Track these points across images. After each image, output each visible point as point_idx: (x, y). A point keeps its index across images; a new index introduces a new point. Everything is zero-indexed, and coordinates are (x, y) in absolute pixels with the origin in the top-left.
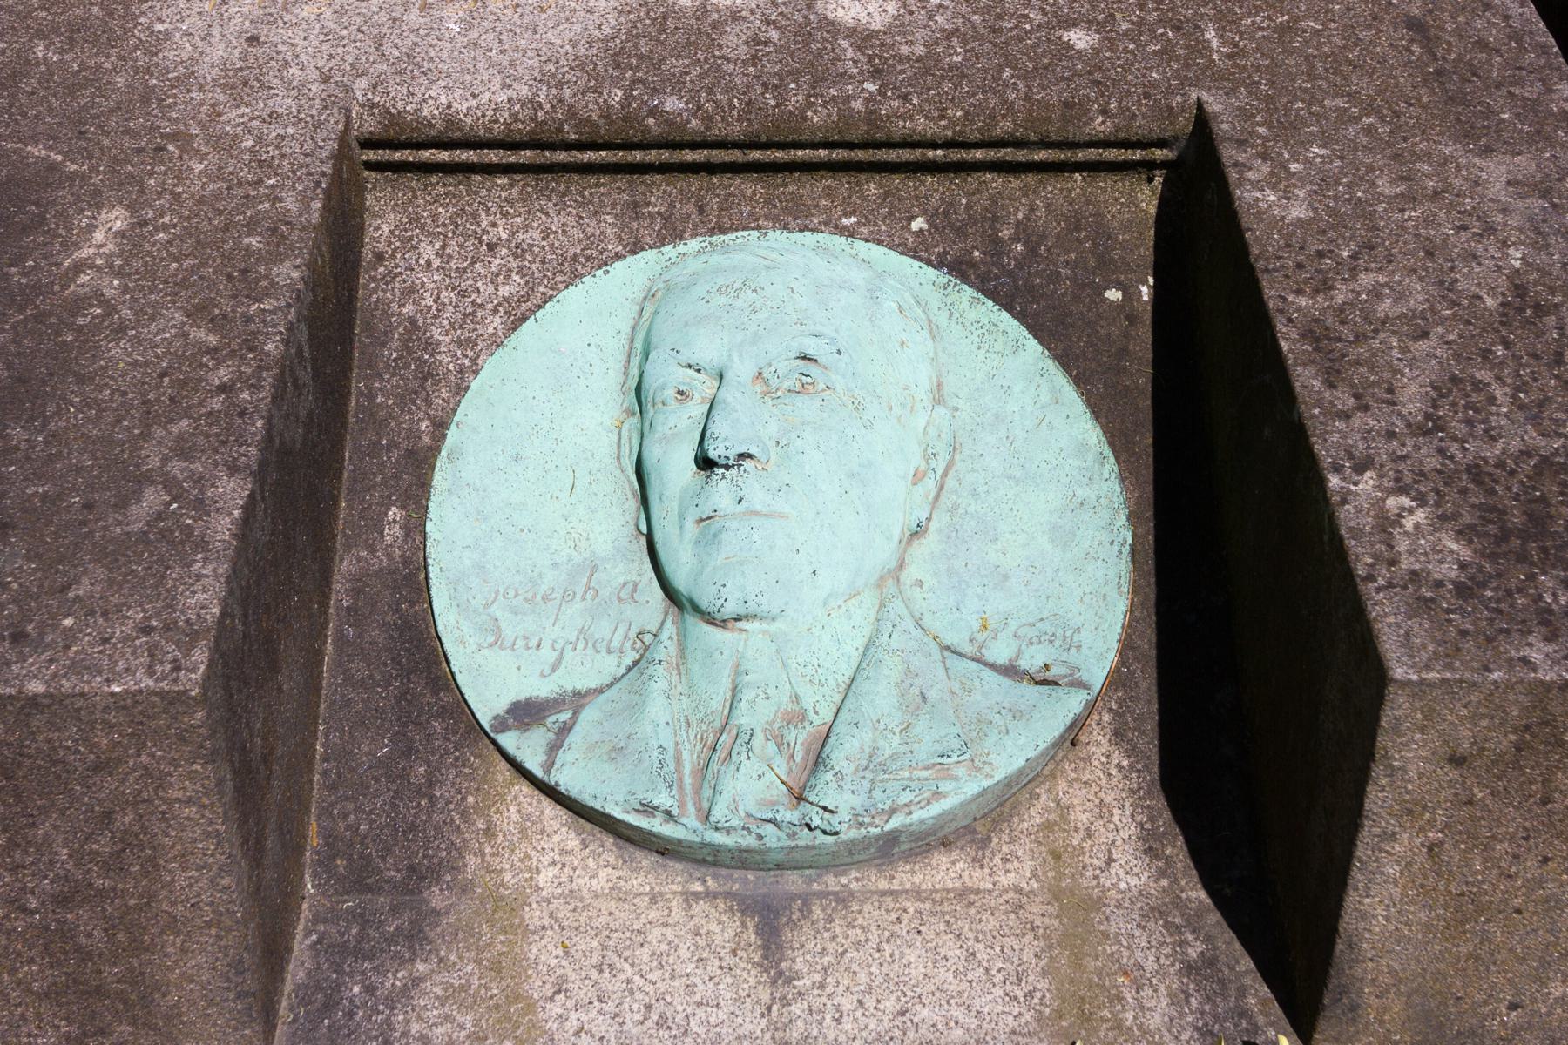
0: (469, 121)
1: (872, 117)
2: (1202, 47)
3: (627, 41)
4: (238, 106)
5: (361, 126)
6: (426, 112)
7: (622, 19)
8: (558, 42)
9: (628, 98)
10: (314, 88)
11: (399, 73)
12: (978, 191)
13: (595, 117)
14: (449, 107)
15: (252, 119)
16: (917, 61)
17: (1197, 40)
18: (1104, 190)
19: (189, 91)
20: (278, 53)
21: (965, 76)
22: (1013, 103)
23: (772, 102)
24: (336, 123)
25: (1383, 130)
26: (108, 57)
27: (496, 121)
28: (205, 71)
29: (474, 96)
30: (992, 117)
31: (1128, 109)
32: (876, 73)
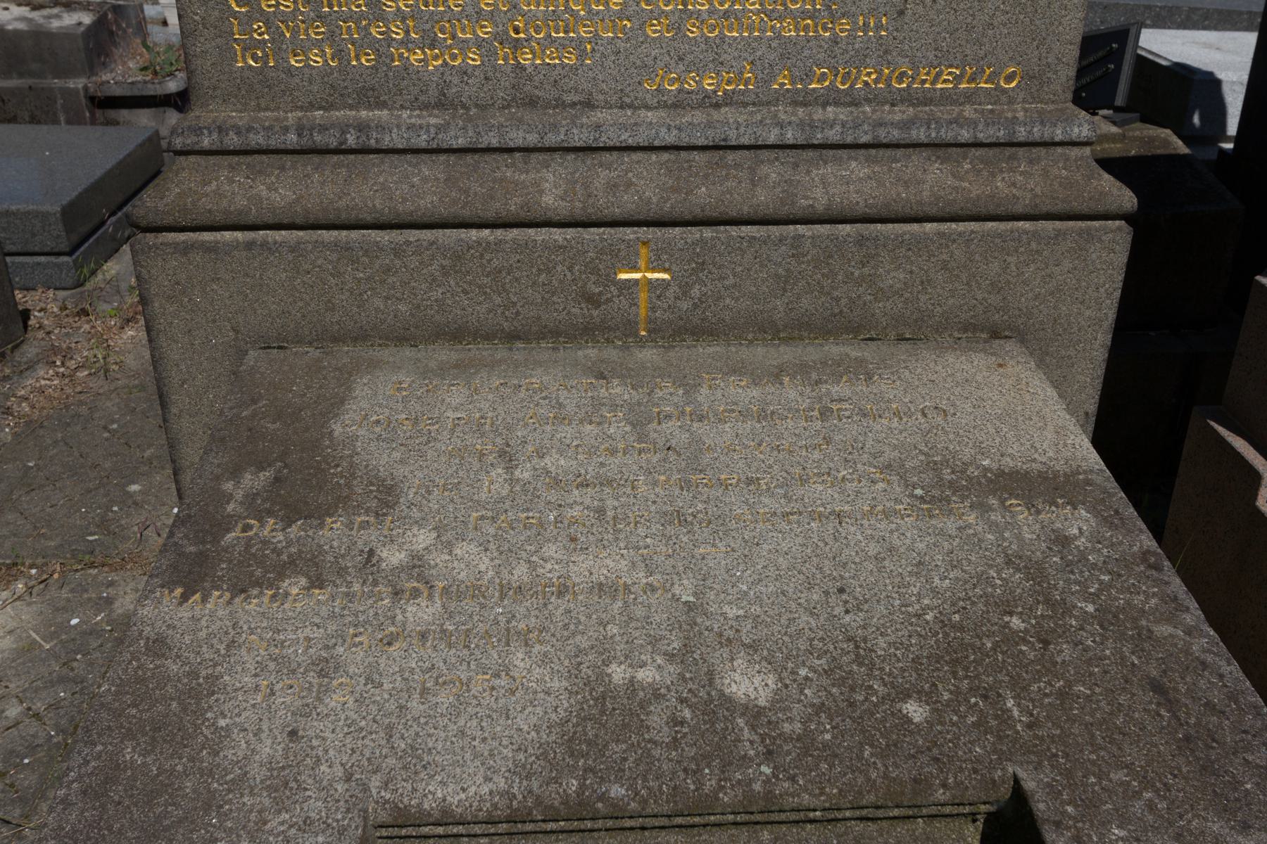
0: (459, 810)
1: (769, 795)
2: (1005, 717)
3: (578, 725)
4: (279, 812)
5: (376, 817)
6: (426, 806)
7: (572, 701)
8: (526, 728)
9: (582, 787)
10: (339, 788)
11: (405, 768)
12: (846, 833)
13: (556, 803)
14: (444, 800)
15: (291, 826)
16: (798, 740)
17: (1001, 709)
18: (939, 830)
19: (242, 795)
20: (312, 748)
21: (836, 756)
22: (875, 781)
23: (692, 787)
24: (357, 828)
25: (1162, 805)
26: (180, 758)
27: (481, 810)
28: (257, 773)
29: (463, 790)
30: (860, 793)
31: (962, 783)
32: (769, 754)
